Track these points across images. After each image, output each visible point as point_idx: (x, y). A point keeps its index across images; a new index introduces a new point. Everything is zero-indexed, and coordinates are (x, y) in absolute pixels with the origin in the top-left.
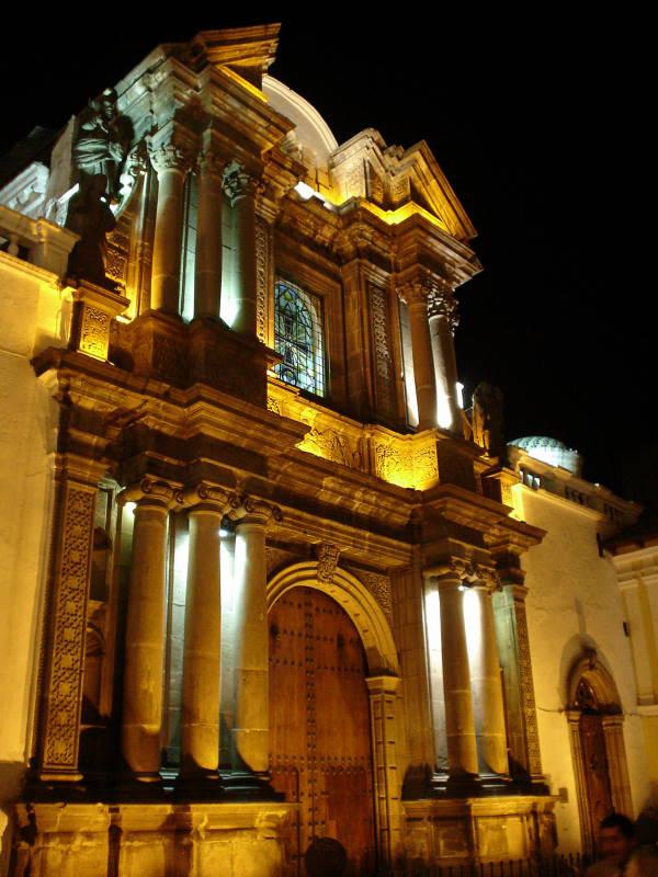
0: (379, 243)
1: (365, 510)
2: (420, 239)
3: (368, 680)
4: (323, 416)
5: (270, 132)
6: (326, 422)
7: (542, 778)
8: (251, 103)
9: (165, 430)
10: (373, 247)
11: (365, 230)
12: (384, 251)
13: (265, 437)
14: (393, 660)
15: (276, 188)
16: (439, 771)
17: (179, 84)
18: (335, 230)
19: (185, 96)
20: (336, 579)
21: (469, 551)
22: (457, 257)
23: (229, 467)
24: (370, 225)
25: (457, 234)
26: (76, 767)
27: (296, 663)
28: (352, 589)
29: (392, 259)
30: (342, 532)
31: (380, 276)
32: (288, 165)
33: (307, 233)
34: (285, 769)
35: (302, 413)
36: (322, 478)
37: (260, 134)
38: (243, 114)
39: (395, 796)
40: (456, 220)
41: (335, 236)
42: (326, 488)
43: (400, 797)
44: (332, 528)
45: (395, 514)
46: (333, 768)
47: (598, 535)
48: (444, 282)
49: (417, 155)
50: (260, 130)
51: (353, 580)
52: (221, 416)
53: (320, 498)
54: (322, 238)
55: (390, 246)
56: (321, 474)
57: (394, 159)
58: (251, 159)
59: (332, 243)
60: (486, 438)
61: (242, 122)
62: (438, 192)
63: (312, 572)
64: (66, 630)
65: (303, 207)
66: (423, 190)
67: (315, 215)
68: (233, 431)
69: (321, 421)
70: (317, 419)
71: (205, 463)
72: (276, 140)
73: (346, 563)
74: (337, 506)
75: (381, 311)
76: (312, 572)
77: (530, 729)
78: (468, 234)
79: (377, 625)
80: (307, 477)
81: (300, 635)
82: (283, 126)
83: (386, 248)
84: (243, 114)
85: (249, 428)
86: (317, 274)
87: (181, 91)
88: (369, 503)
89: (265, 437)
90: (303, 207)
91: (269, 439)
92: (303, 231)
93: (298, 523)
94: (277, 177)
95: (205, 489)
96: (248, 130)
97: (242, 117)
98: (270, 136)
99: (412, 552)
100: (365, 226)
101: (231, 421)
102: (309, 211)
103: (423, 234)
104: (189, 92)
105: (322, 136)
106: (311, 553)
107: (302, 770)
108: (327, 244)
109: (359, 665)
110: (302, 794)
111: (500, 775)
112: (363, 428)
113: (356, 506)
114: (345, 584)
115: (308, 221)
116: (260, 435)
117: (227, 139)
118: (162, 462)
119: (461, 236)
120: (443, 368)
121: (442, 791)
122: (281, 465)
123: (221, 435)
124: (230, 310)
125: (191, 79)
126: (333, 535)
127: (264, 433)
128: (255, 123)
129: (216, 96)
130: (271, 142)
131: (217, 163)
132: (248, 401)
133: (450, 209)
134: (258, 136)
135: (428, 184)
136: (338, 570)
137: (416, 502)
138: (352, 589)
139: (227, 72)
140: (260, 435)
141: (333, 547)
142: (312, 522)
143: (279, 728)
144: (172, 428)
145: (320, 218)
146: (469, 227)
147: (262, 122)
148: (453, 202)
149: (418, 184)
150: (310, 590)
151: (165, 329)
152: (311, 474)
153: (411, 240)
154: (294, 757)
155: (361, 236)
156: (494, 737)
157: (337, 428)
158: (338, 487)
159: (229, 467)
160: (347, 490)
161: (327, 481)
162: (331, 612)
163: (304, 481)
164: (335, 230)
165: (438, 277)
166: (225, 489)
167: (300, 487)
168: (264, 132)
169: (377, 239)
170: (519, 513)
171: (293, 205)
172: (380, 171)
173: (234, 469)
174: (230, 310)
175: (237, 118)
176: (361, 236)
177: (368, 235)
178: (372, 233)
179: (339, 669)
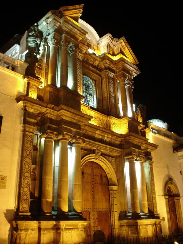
0: (111, 65)
3: (109, 187)
4: (96, 114)
6: (97, 116)
7: (158, 214)
8: (76, 27)
13: (80, 119)
14: (116, 181)
15: (83, 50)
16: (129, 212)
17: (55, 21)
19: (57, 25)
20: (100, 159)
22: (133, 69)
24: (109, 60)
25: (133, 63)
26: (29, 211)
27: (89, 182)
28: (104, 162)
31: (112, 75)
32: (86, 44)
33: (91, 63)
36: (96, 131)
37: (78, 35)
40: (133, 58)
41: (99, 63)
47: (173, 147)
48: (130, 76)
49: (122, 41)
50: (78, 34)
51: (105, 159)
52: (68, 114)
53: (96, 136)
54: (95, 64)
60: (142, 120)
61: (73, 32)
63: (93, 157)
64: (26, 173)
65: (90, 56)
69: (95, 115)
73: (103, 154)
74: (100, 139)
76: (93, 157)
77: (154, 201)
80: (92, 131)
82: (84, 33)
83: (113, 67)
85: (76, 117)
89: (80, 119)
90: (90, 56)
91: (81, 120)
93: (89, 143)
94: (83, 47)
97: (73, 31)
101: (71, 115)
102: (92, 57)
103: (124, 63)
106: (93, 152)
108: (97, 66)
109: (107, 183)
111: (146, 213)
117: (69, 37)
121: (130, 218)
122: (85, 127)
123: (68, 119)
125: (59, 20)
130: (81, 37)
133: (131, 56)
134: (78, 36)
135: (125, 48)
136: (101, 157)
137: (122, 137)
139: (69, 18)
142: (93, 143)
143: (84, 200)
144: (54, 117)
146: (137, 61)
147: (78, 32)
149: (122, 49)
150: (93, 162)
155: (106, 63)
160: (103, 134)
162: (99, 168)
163: (91, 132)
167: (90, 133)
168: (79, 35)
172: (112, 45)
173: (72, 129)
174: (70, 84)
175: (72, 31)
176: (106, 63)
177: (108, 63)
178: (109, 63)
179: (101, 184)
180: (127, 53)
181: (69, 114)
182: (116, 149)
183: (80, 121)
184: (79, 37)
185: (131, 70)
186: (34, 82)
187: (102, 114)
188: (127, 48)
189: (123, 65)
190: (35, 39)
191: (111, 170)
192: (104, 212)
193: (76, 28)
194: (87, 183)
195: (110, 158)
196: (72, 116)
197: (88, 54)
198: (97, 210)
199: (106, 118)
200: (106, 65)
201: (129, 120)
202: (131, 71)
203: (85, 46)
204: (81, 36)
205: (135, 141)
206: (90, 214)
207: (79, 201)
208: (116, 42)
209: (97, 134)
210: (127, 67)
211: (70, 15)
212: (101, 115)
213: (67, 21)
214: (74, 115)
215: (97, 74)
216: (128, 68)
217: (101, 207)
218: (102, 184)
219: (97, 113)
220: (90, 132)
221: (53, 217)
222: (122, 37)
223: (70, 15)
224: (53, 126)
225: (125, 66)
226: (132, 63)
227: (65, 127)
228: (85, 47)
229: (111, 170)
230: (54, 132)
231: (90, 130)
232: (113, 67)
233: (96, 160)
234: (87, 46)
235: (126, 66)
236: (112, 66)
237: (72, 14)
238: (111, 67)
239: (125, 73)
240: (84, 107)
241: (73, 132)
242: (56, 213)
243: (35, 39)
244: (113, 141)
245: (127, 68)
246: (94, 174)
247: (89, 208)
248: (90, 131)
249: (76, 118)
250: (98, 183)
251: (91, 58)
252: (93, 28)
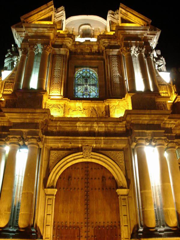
0: (112, 42)
1: (102, 130)
2: (122, 33)
4: (85, 103)
6: (87, 105)
8: (39, 26)
9: (5, 125)
10: (110, 44)
11: (104, 41)
12: (115, 43)
13: (34, 117)
15: (66, 44)
21: (149, 133)
22: (141, 31)
24: (105, 38)
25: (144, 25)
27: (80, 188)
28: (102, 159)
30: (87, 140)
31: (115, 52)
32: (66, 36)
33: (88, 51)
34: (74, 227)
36: (76, 124)
37: (47, 32)
39: (125, 237)
40: (141, 20)
41: (99, 47)
43: (130, 237)
45: (117, 128)
46: (99, 227)
48: (138, 42)
50: (46, 31)
51: (101, 155)
52: (15, 115)
53: (79, 130)
54: (94, 50)
55: (117, 41)
56: (75, 122)
57: (117, 15)
58: (44, 41)
59: (98, 50)
60: (175, 88)
66: (127, 18)
67: (87, 45)
68: (22, 118)
69: (85, 105)
70: (83, 105)
71: (11, 130)
72: (53, 32)
73: (95, 150)
74: (88, 131)
75: (116, 62)
78: (147, 22)
80: (69, 125)
81: (82, 179)
83: (116, 42)
84: (39, 30)
85: (26, 116)
86: (93, 61)
87: (21, 34)
88: (101, 127)
89: (34, 117)
90: (83, 45)
91: (36, 117)
92: (87, 51)
93: (66, 141)
95: (9, 138)
97: (39, 31)
98: (50, 31)
99: (128, 140)
101: (19, 116)
103: (123, 31)
104: (24, 33)
105: (103, 23)
107: (82, 227)
108: (97, 51)
109: (110, 186)
110: (82, 236)
112: (104, 102)
114: (98, 158)
115: (87, 48)
116: (32, 117)
117: (34, 39)
118: (2, 134)
119: (146, 24)
120: (141, 70)
121: (141, 235)
122: (57, 124)
123: (18, 121)
124: (34, 84)
126: (84, 142)
127: (32, 116)
129: (29, 30)
130: (52, 33)
131: (31, 47)
132: (21, 108)
133: (138, 18)
134: (46, 33)
135: (127, 15)
136: (93, 153)
137: (123, 120)
139: (37, 23)
140: (32, 117)
141: (88, 146)
142: (74, 139)
143: (70, 213)
144: (7, 124)
146: (147, 19)
147: (45, 29)
148: (138, 15)
149: (124, 17)
151: (9, 97)
152: (69, 124)
153: (120, 35)
154: (78, 223)
156: (167, 210)
158: (84, 125)
160: (89, 125)
161: (78, 124)
162: (98, 168)
163: (68, 126)
165: (134, 42)
167: (68, 129)
168: (48, 31)
169: (111, 41)
171: (78, 46)
173: (22, 130)
174: (34, 84)
175: (38, 32)
177: (106, 42)
179: (103, 189)
180: (131, 18)
181: (16, 116)
182: (118, 138)
183: (35, 119)
184: (49, 33)
185: (139, 34)
186: (163, 99)
187: (93, 101)
189: (124, 33)
190: (11, 59)
191: (115, 167)
192: (107, 226)
193: (40, 27)
194: (97, 190)
195: (112, 152)
196: (21, 116)
197: (79, 45)
198: (95, 225)
199: (103, 104)
201: (133, 95)
202: (140, 35)
203: (66, 38)
205: (141, 120)
206: (80, 230)
209: (79, 127)
210: (131, 33)
211: (37, 19)
212: (93, 103)
213: (120, 28)
214: (23, 115)
216: (133, 34)
217: (102, 220)
218: (104, 188)
220: (67, 127)
221: (33, 234)
223: (37, 19)
224: (3, 133)
225: (128, 33)
227: (12, 130)
229: (115, 167)
231: (65, 125)
232: (116, 42)
234: (68, 37)
235: (129, 33)
236: (113, 42)
237: (40, 17)
239: (129, 42)
240: (62, 102)
241: (24, 133)
243: (11, 59)
244: (112, 129)
245: (131, 35)
246: (90, 178)
247: (79, 222)
248: (66, 126)
249: (28, 117)
250: (97, 188)
251: (86, 47)
252: (102, 18)
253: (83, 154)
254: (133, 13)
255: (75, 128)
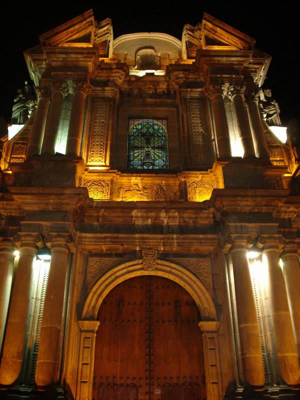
0: (191, 76)
4: (145, 178)
5: (87, 57)
6: (150, 182)
8: (70, 51)
9: (13, 214)
10: (188, 80)
11: (178, 74)
12: (196, 79)
14: (213, 310)
15: (114, 80)
17: (38, 62)
18: (166, 83)
19: (44, 66)
20: (159, 267)
22: (239, 59)
23: (38, 222)
24: (180, 70)
25: (244, 47)
28: (174, 271)
29: (204, 80)
31: (196, 93)
33: (151, 92)
35: (132, 181)
36: (131, 212)
37: (82, 61)
38: (69, 58)
41: (168, 85)
42: (136, 217)
44: (143, 238)
50: (81, 59)
51: (173, 265)
52: (29, 199)
54: (161, 90)
55: (199, 75)
59: (168, 90)
60: (295, 152)
61: (72, 61)
62: (224, 33)
63: (139, 267)
65: (141, 81)
67: (150, 82)
69: (146, 182)
73: (164, 256)
76: (139, 267)
79: (199, 291)
83: (197, 77)
88: (174, 217)
90: (141, 81)
91: (65, 201)
92: (148, 92)
94: (112, 75)
96: (75, 63)
97: (69, 59)
100: (177, 73)
102: (146, 81)
111: (290, 386)
113: (166, 221)
114: (168, 269)
115: (148, 86)
122: (99, 212)
123: (35, 208)
125: (42, 58)
126: (145, 242)
128: (78, 58)
133: (233, 37)
134: (81, 63)
135: (216, 32)
137: (209, 207)
138: (174, 271)
142: (128, 238)
145: (153, 82)
146: (248, 39)
148: (233, 32)
149: (211, 35)
154: (134, 378)
155: (177, 78)
157: (160, 182)
159: (38, 222)
160: (153, 214)
163: (117, 217)
164: (166, 83)
166: (33, 233)
168: (85, 59)
169: (188, 75)
170: (207, 197)
173: (41, 223)
175: (67, 61)
176: (177, 78)
177: (181, 76)
178: (183, 74)
185: (235, 63)
188: (218, 28)
193: (71, 53)
200: (178, 81)
202: (236, 65)
204: (88, 59)
207: (42, 361)
208: (199, 32)
215: (167, 105)
219: (147, 177)
222: (106, 18)
226: (241, 47)
228: (115, 73)
230: (10, 238)
232: (197, 77)
233: (147, 270)
234: (117, 69)
235: (219, 61)
238: (190, 80)
239: (219, 76)
242: (243, 389)
253: (142, 263)
254: (63, 28)
255: (130, 219)
